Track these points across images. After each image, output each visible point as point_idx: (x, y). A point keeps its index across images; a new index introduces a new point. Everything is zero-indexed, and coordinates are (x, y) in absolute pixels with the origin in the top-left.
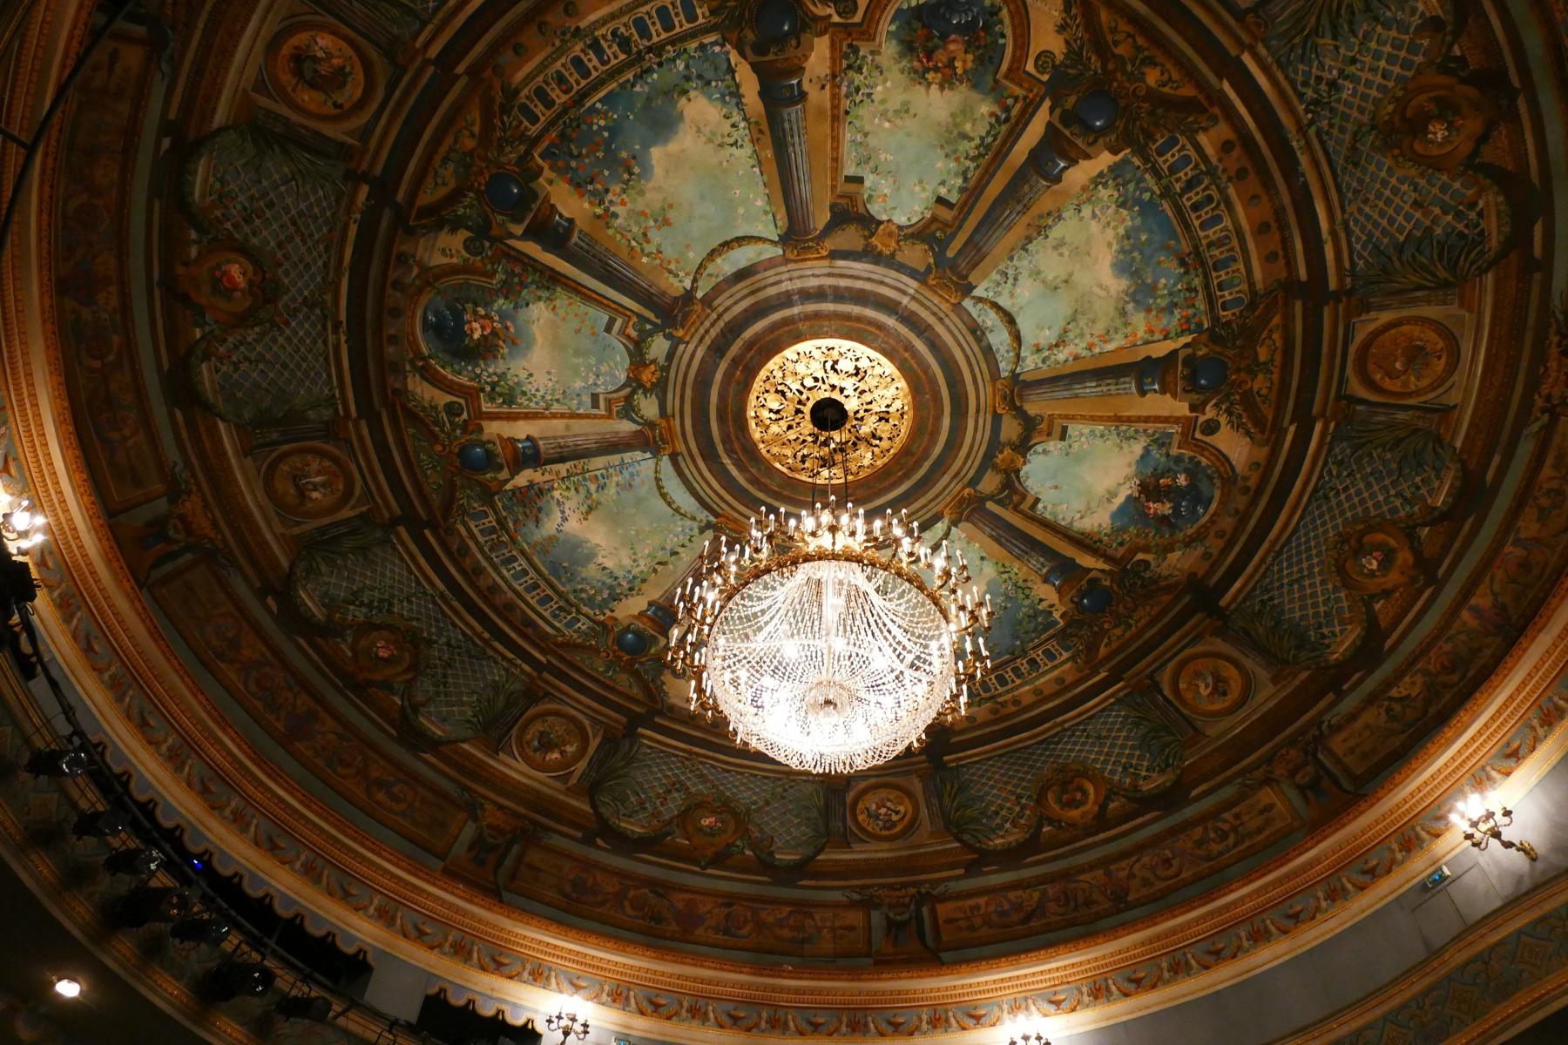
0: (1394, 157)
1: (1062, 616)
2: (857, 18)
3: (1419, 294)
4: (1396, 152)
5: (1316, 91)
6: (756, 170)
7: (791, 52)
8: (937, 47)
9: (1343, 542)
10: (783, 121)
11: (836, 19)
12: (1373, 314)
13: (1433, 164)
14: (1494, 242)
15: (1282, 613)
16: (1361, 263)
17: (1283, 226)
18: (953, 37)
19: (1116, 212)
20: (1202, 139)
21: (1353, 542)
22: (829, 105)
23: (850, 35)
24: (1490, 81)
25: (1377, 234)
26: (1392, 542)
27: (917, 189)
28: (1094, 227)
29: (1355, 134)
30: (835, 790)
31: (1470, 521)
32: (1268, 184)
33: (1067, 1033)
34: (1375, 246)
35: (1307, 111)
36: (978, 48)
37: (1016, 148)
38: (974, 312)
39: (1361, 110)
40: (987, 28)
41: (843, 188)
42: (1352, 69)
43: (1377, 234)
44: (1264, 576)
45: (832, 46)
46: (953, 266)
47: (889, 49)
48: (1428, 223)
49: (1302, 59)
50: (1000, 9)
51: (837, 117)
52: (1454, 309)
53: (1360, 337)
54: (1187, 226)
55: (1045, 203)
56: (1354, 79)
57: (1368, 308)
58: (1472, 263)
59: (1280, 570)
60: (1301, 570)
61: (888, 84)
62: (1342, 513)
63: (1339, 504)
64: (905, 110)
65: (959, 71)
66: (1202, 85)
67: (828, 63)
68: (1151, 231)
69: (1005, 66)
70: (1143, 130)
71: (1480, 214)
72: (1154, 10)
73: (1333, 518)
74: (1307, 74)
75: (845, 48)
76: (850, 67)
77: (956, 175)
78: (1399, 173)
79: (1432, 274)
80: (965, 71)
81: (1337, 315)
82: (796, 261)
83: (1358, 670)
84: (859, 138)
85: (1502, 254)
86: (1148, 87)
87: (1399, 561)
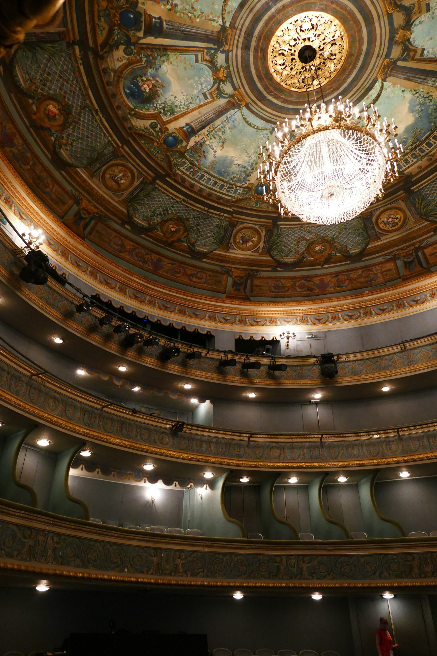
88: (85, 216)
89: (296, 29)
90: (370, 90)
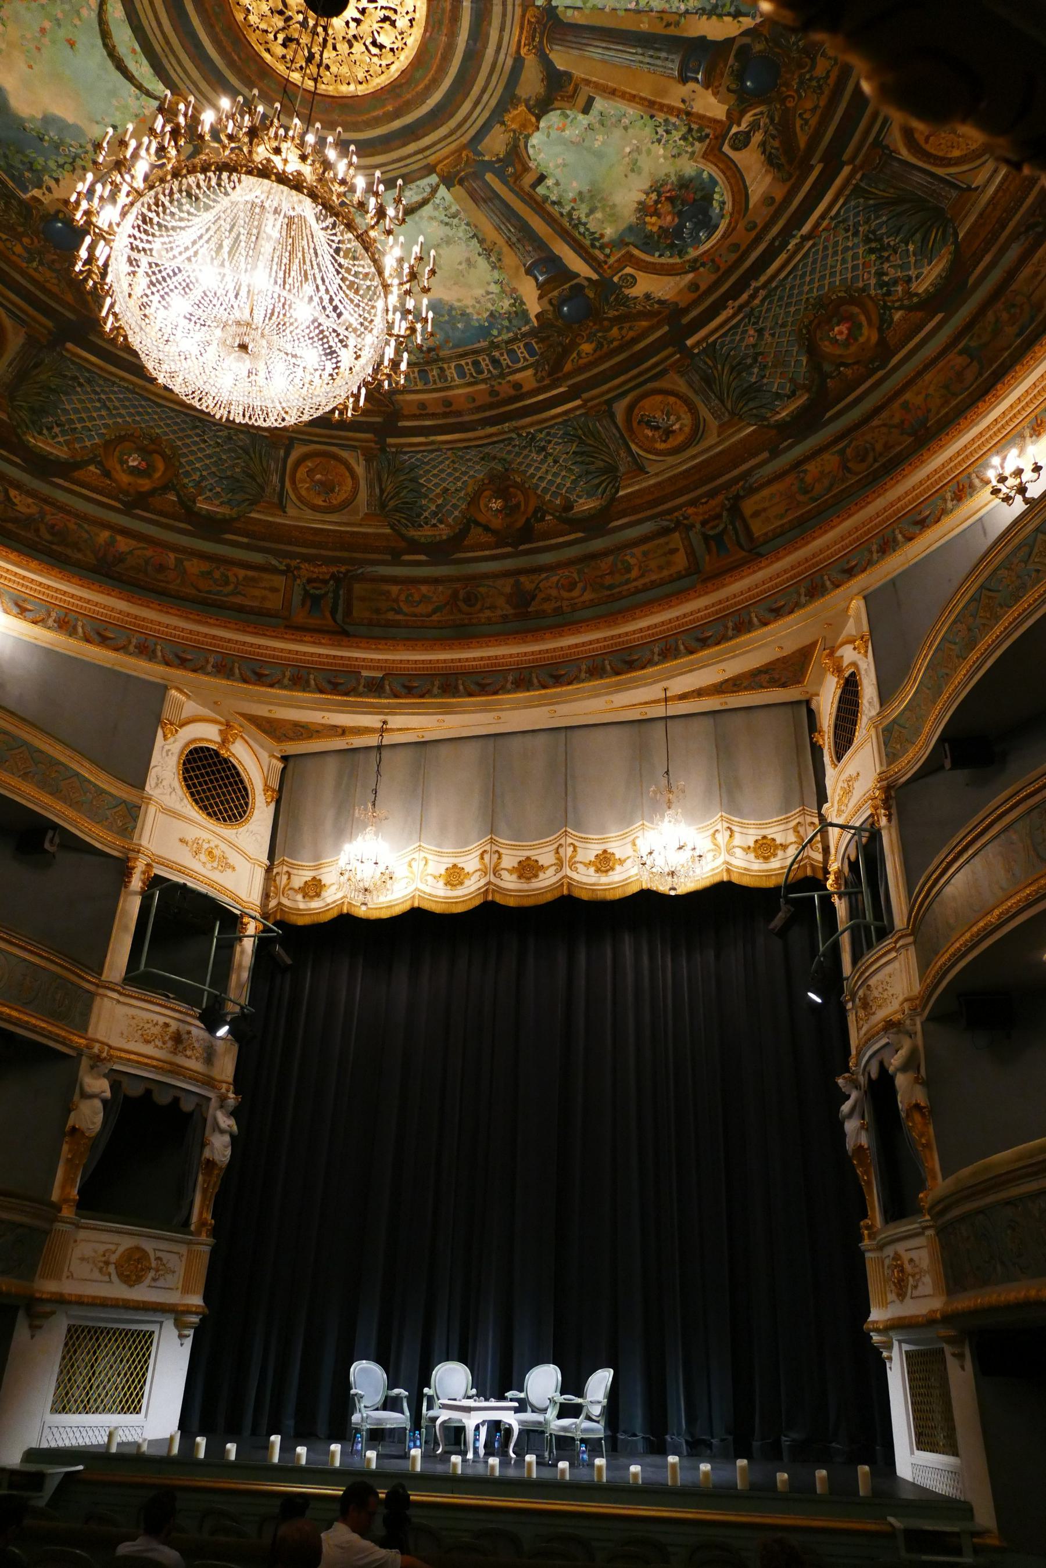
0: (483, 480)
1: (34, 198)
2: (726, 148)
3: (377, 490)
4: (486, 481)
5: (541, 440)
6: (632, 6)
7: (727, 81)
8: (674, 207)
9: (151, 439)
10: (669, 52)
11: (735, 129)
12: (362, 462)
13: (474, 500)
14: (413, 533)
15: (66, 394)
16: (406, 457)
17: (445, 415)
18: (677, 220)
19: (487, 310)
20: (530, 372)
21: (152, 447)
22: (666, 102)
23: (716, 138)
24: (526, 534)
25: (427, 468)
26: (157, 475)
27: (560, 161)
28: (479, 292)
29: (505, 460)
30: (255, 449)
31: (190, 527)
32: (480, 409)
33: (15, 634)
34: (418, 466)
35: (528, 433)
36: (659, 237)
37: (566, 248)
38: (424, 183)
39: (520, 464)
40: (672, 246)
41: (585, 91)
42: (550, 460)
43: (427, 468)
44: (106, 380)
45: (716, 121)
46: (477, 176)
47: (689, 168)
48: (431, 496)
49: (566, 434)
50: (681, 257)
51: (652, 106)
52: (364, 509)
53: (344, 454)
54: (462, 356)
55: (510, 259)
56: (542, 462)
57: (368, 460)
58: (399, 521)
59: (115, 393)
60: (116, 408)
61: (662, 160)
62: (181, 439)
63: (189, 436)
64: (634, 168)
65: (648, 219)
66: (569, 375)
67: (701, 112)
68: (463, 332)
69: (636, 252)
70: (548, 337)
71: (434, 525)
72: (635, 353)
73: (174, 432)
74: (555, 436)
75: (707, 131)
76: (690, 130)
77: (561, 196)
78: (471, 482)
79: (392, 498)
80: (645, 223)
81: (366, 441)
82: (523, 16)
83: (23, 460)
84: (626, 121)
85: (403, 537)
86: (580, 344)
87: (141, 481)
88: (323, 592)
89: (395, 11)
90: (152, 66)
